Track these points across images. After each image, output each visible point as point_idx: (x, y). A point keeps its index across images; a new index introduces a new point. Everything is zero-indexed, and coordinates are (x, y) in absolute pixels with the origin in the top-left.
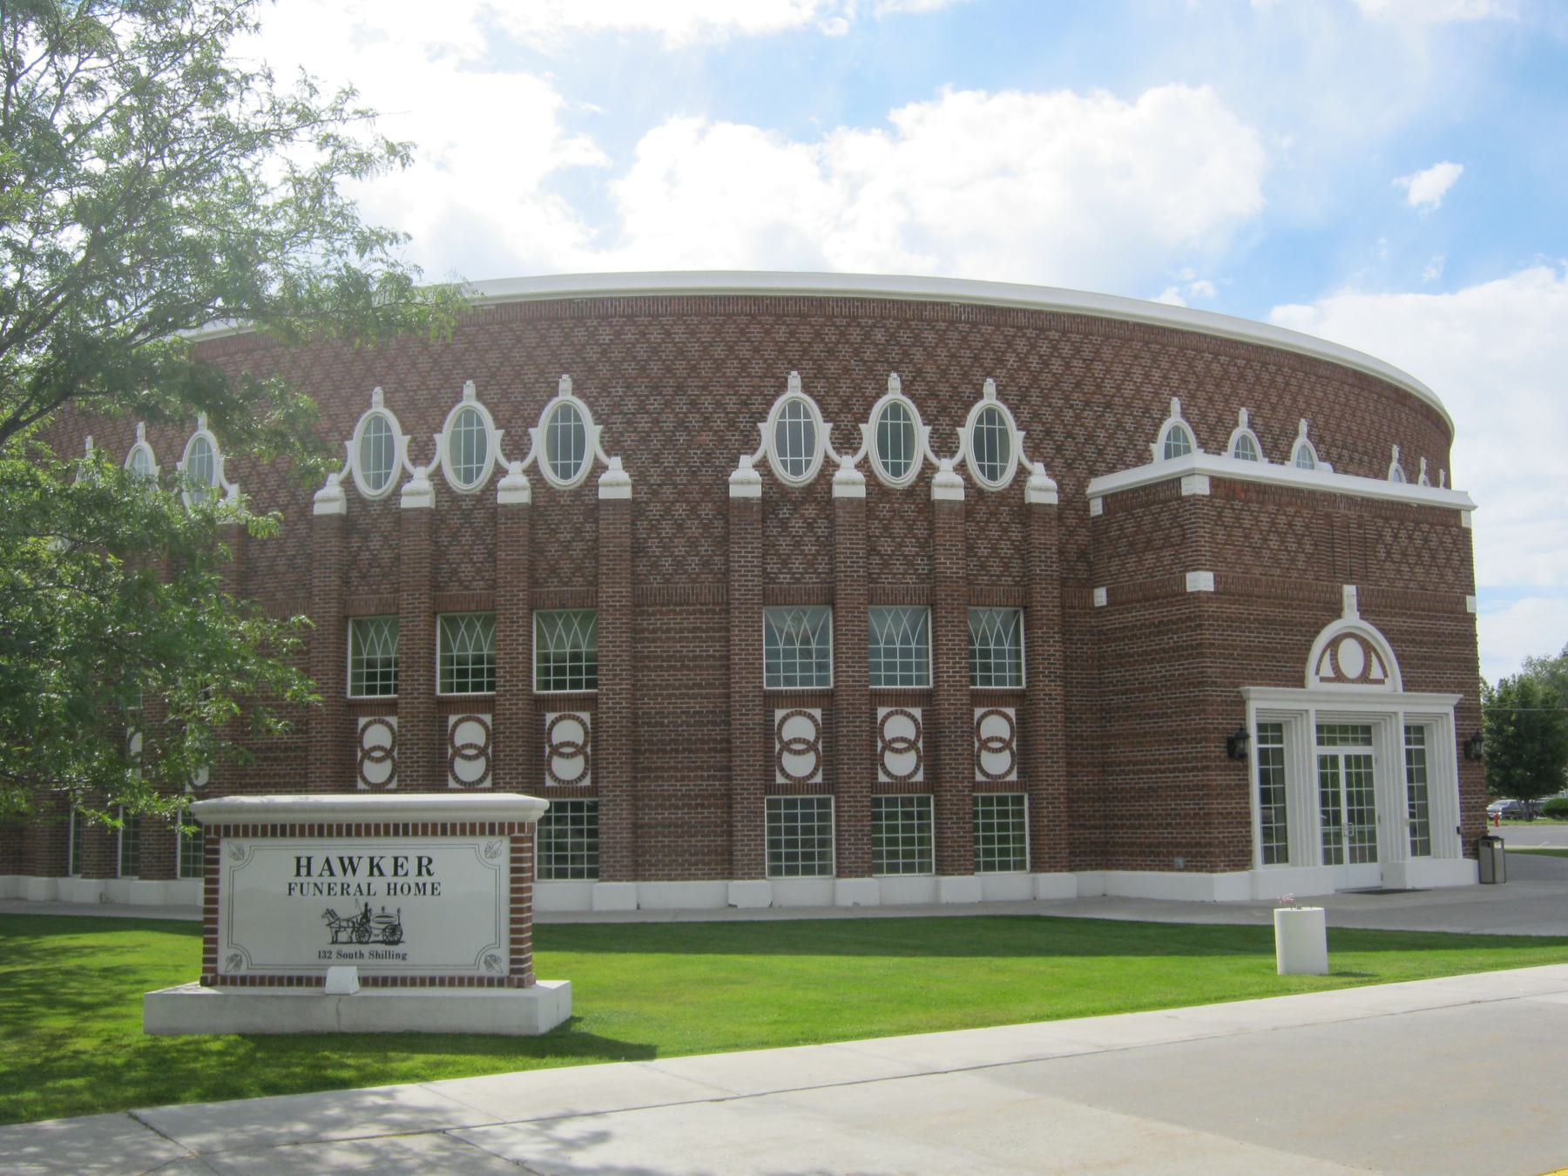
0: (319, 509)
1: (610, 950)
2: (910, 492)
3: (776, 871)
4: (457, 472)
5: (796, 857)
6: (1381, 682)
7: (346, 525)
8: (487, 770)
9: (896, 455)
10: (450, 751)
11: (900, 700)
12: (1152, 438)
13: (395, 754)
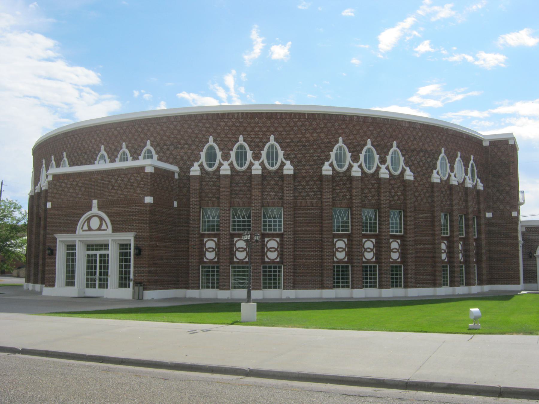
0: (192, 174)
1: (201, 312)
2: (373, 174)
3: (265, 287)
4: (207, 164)
5: (367, 283)
6: (105, 230)
7: (200, 179)
8: (216, 255)
9: (272, 160)
10: (235, 249)
11: (394, 237)
12: (437, 160)
13: (334, 250)
